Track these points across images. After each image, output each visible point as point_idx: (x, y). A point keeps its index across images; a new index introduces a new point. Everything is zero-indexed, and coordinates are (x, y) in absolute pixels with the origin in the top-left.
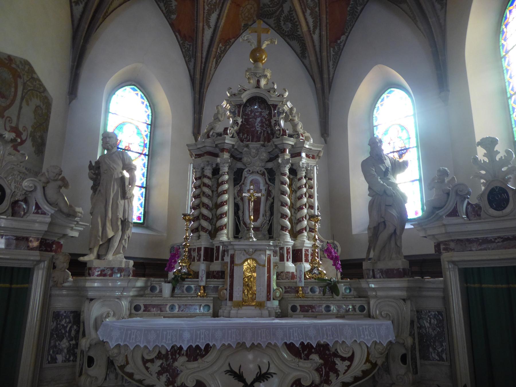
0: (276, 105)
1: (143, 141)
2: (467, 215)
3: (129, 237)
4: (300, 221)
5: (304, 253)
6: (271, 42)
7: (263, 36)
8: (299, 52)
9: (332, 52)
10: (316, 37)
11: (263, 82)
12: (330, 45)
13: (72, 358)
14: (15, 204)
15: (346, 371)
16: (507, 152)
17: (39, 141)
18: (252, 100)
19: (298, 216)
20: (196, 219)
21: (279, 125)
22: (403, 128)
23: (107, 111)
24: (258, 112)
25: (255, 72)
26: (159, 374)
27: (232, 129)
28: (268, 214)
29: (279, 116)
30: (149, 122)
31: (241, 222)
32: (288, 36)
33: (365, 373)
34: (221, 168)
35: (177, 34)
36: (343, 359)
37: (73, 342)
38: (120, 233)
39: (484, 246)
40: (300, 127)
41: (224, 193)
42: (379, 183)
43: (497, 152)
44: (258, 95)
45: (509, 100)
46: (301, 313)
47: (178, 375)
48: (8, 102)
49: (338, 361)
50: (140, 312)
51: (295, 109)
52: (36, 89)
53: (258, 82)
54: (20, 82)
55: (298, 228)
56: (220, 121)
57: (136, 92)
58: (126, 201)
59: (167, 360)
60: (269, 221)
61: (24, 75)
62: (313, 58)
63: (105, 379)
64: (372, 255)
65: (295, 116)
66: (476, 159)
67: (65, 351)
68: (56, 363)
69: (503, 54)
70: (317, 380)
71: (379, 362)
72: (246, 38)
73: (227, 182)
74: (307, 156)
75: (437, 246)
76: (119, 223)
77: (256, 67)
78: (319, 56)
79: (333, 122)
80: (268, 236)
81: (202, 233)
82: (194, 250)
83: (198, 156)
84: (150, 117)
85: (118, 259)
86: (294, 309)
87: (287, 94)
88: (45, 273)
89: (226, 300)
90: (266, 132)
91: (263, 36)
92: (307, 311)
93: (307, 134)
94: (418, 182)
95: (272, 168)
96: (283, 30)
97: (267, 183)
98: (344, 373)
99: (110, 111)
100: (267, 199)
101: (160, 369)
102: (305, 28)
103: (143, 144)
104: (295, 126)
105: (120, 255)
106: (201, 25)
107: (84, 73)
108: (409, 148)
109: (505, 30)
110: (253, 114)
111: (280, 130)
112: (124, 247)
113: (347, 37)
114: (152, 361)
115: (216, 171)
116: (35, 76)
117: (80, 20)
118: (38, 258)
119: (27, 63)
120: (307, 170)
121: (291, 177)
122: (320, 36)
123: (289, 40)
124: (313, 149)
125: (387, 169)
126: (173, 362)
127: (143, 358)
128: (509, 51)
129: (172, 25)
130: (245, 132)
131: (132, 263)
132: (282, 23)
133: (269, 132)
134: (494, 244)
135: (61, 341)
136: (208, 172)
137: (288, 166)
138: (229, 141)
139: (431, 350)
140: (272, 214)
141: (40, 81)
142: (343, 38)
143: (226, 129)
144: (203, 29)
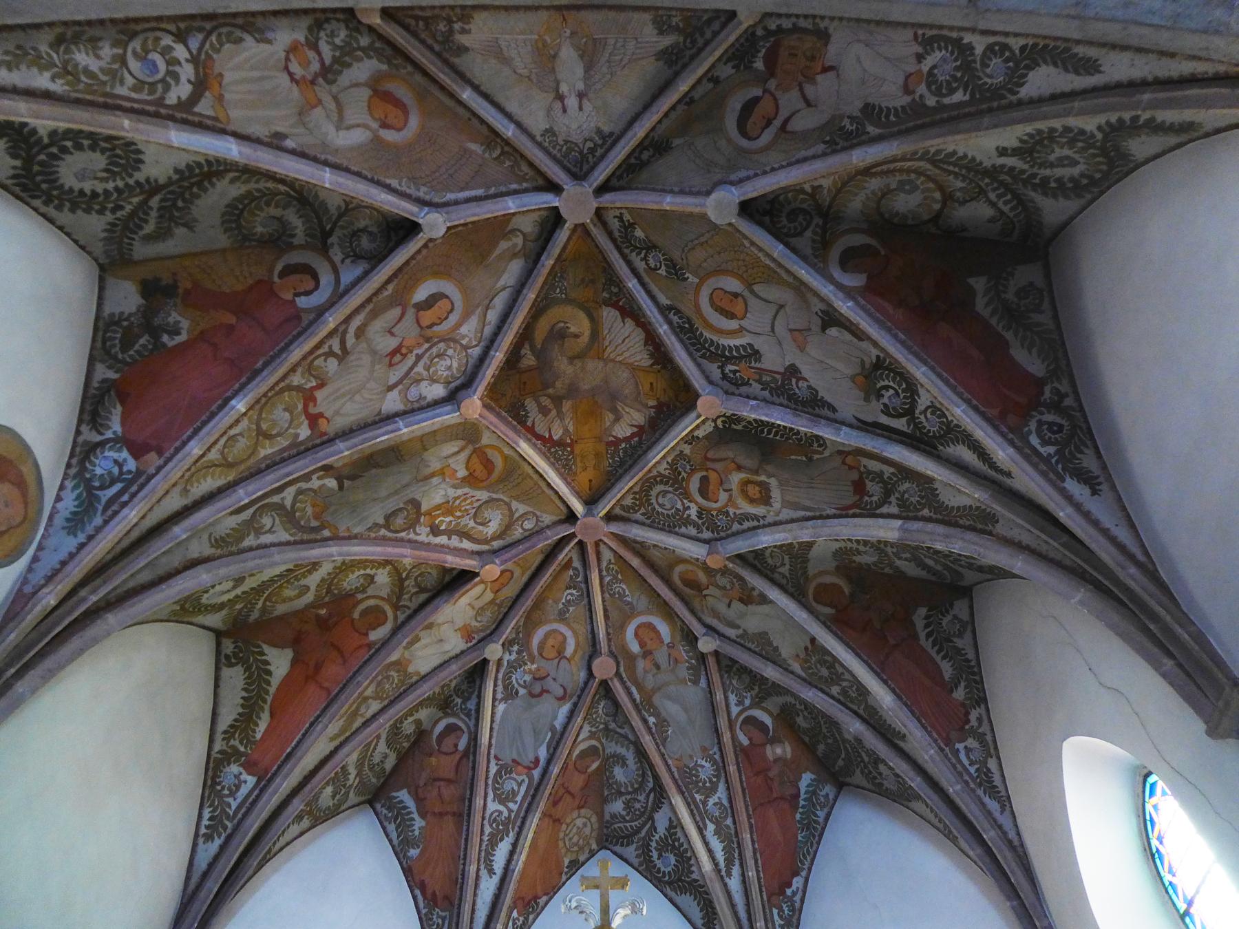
6: (633, 911)
7: (614, 896)
9: (776, 917)
10: (734, 884)
12: (769, 901)
32: (670, 883)
35: (418, 892)
69: (1182, 907)
72: (574, 904)
91: (614, 896)
106: (473, 869)
117: (205, 875)
129: (408, 872)
132: (655, 854)
142: (797, 882)
144: (478, 877)
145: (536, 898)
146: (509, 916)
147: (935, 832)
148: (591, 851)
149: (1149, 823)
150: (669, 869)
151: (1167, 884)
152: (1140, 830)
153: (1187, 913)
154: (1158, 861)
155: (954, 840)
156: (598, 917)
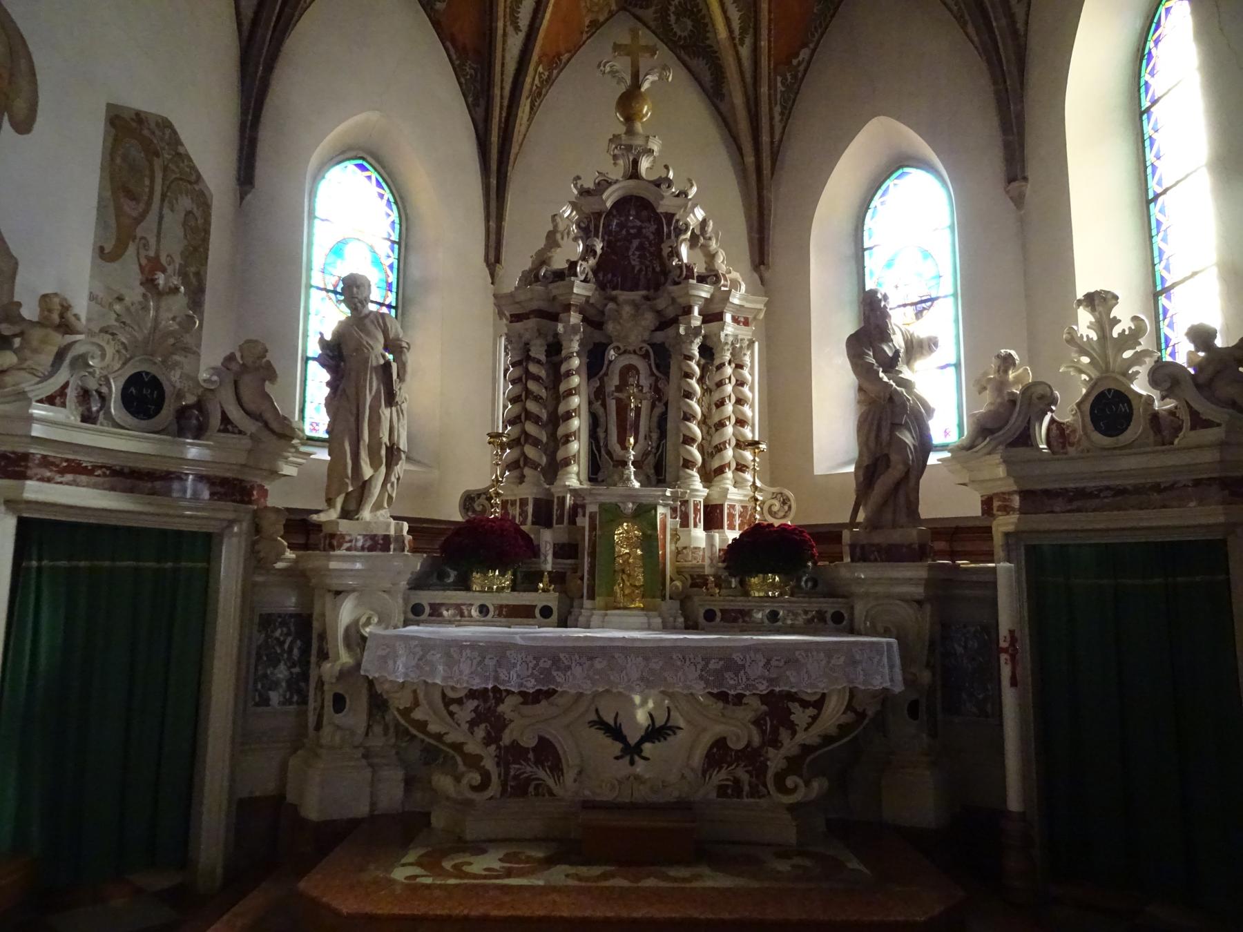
0: (673, 215)
1: (384, 276)
2: (1048, 443)
3: (398, 479)
4: (720, 449)
5: (726, 511)
6: (660, 78)
7: (644, 62)
8: (708, 85)
9: (779, 84)
10: (745, 51)
11: (645, 164)
12: (775, 68)
13: (295, 698)
14: (182, 413)
15: (810, 725)
16: (1135, 318)
17: (194, 280)
18: (622, 204)
19: (716, 440)
20: (515, 443)
21: (678, 255)
22: (926, 254)
23: (312, 216)
24: (633, 227)
25: (628, 142)
26: (473, 724)
27: (584, 264)
28: (655, 436)
29: (677, 236)
30: (395, 237)
31: (603, 452)
32: (683, 47)
33: (843, 729)
34: (564, 344)
35: (448, 44)
36: (805, 704)
37: (296, 670)
38: (383, 469)
39: (1076, 505)
40: (721, 264)
41: (572, 394)
42: (881, 379)
43: (1116, 321)
44: (635, 193)
45: (1152, 206)
46: (722, 624)
47: (505, 726)
48: (142, 206)
49: (795, 707)
50: (424, 616)
51: (711, 223)
52: (186, 178)
53: (635, 163)
54: (158, 163)
55: (716, 464)
56: (559, 246)
57: (368, 173)
58: (394, 409)
59: (486, 701)
60: (658, 448)
61: (163, 149)
62: (738, 100)
63: (367, 734)
64: (861, 517)
65: (710, 239)
66: (1072, 332)
67: (284, 684)
68: (268, 705)
69: (1145, 104)
70: (756, 740)
71: (870, 713)
72: (608, 69)
73: (578, 371)
74: (735, 320)
75: (987, 503)
76: (383, 452)
77: (630, 132)
78: (751, 92)
79: (777, 238)
80: (654, 478)
81: (527, 471)
82: (513, 503)
83: (516, 318)
84: (397, 226)
85: (381, 519)
86: (710, 616)
87: (693, 191)
88: (243, 544)
89: (582, 597)
90: (650, 269)
91: (644, 62)
92: (735, 620)
93: (735, 275)
94: (952, 369)
95: (663, 343)
96: (675, 34)
97: (652, 374)
98: (806, 729)
99: (317, 214)
100: (653, 406)
101: (473, 715)
102: (722, 33)
103: (384, 285)
104: (711, 257)
105: (382, 512)
106: (500, 24)
107: (266, 134)
108: (937, 298)
109: (1154, 51)
110: (624, 232)
111: (680, 267)
112: (390, 497)
113: (814, 51)
114: (460, 701)
115: (555, 349)
116: (181, 150)
117: (255, 22)
118: (231, 516)
119: (165, 124)
120: (734, 349)
121: (703, 362)
122: (755, 49)
123: (686, 58)
124: (747, 305)
125: (897, 353)
126: (497, 704)
127: (444, 695)
128: (1159, 98)
129: (437, 25)
130: (610, 272)
131: (406, 526)
132: (673, 18)
133: (658, 269)
134: (1097, 501)
135: (275, 667)
136: (538, 351)
137: (698, 341)
138: (580, 289)
139: (964, 696)
140: (663, 434)
141: (190, 160)
142: (804, 54)
143: (573, 265)
144: (505, 35)
145: (559, 55)
146: (536, 71)
147: (948, 14)
148: (610, 11)
149: (1154, 26)
150: (686, 34)
151: (1142, 83)
152: (1141, 34)
153: (1148, 110)
154: (1144, 62)
155: (964, 27)
156: (629, 82)
